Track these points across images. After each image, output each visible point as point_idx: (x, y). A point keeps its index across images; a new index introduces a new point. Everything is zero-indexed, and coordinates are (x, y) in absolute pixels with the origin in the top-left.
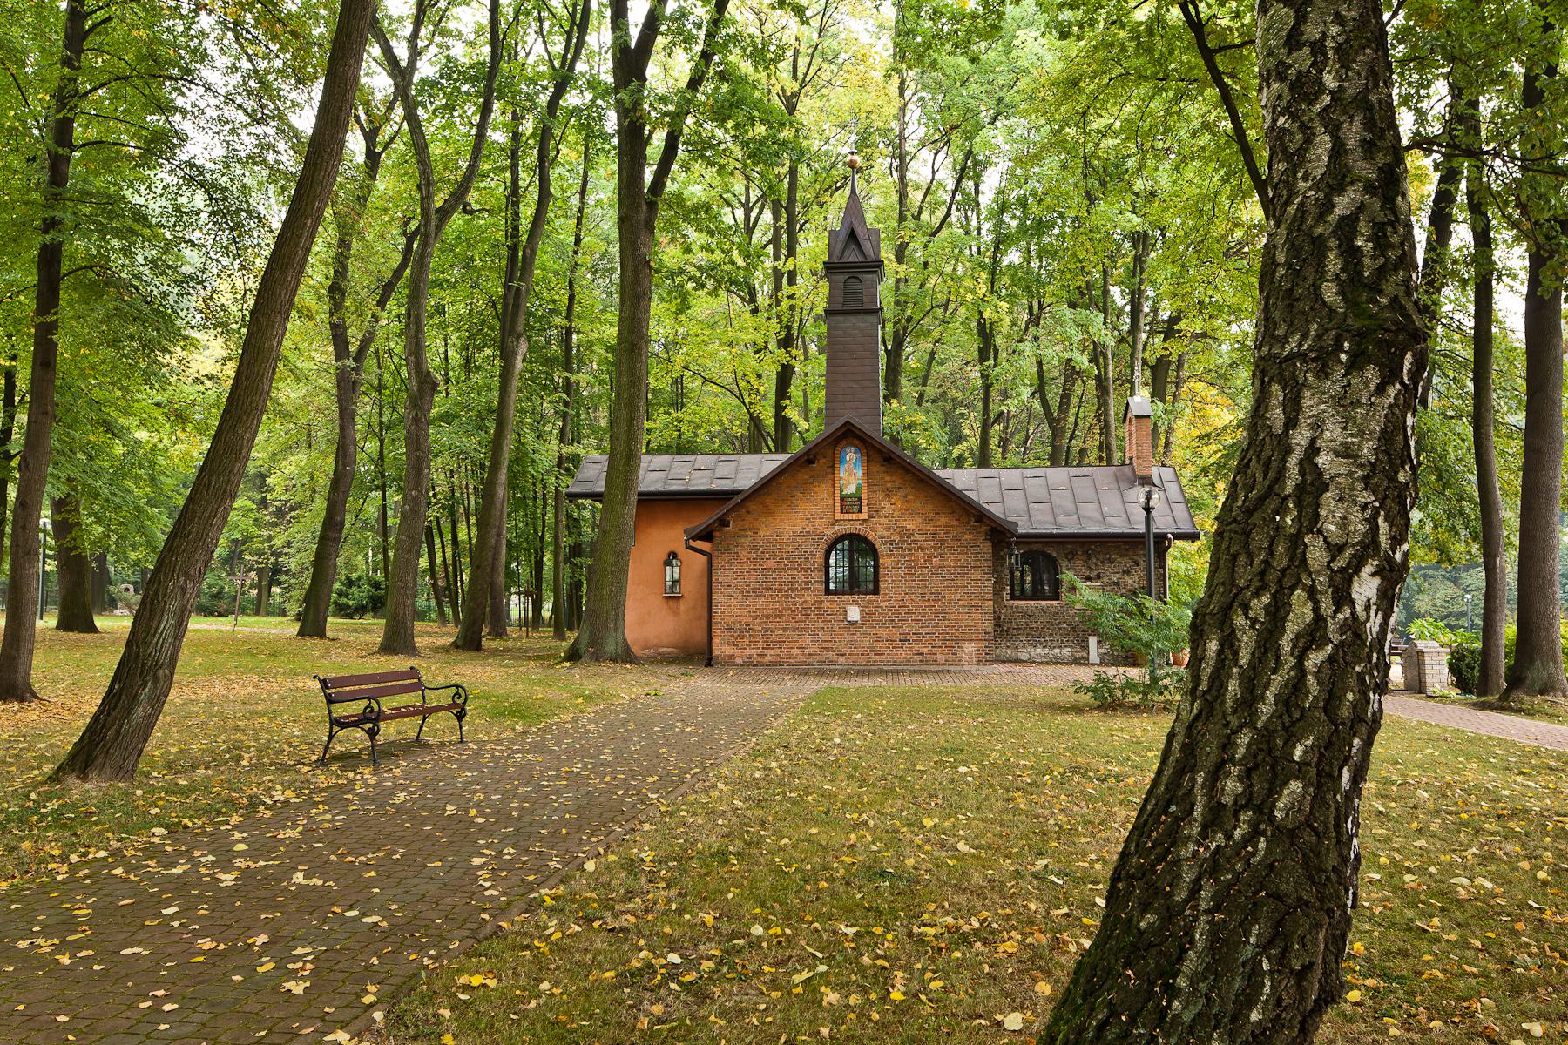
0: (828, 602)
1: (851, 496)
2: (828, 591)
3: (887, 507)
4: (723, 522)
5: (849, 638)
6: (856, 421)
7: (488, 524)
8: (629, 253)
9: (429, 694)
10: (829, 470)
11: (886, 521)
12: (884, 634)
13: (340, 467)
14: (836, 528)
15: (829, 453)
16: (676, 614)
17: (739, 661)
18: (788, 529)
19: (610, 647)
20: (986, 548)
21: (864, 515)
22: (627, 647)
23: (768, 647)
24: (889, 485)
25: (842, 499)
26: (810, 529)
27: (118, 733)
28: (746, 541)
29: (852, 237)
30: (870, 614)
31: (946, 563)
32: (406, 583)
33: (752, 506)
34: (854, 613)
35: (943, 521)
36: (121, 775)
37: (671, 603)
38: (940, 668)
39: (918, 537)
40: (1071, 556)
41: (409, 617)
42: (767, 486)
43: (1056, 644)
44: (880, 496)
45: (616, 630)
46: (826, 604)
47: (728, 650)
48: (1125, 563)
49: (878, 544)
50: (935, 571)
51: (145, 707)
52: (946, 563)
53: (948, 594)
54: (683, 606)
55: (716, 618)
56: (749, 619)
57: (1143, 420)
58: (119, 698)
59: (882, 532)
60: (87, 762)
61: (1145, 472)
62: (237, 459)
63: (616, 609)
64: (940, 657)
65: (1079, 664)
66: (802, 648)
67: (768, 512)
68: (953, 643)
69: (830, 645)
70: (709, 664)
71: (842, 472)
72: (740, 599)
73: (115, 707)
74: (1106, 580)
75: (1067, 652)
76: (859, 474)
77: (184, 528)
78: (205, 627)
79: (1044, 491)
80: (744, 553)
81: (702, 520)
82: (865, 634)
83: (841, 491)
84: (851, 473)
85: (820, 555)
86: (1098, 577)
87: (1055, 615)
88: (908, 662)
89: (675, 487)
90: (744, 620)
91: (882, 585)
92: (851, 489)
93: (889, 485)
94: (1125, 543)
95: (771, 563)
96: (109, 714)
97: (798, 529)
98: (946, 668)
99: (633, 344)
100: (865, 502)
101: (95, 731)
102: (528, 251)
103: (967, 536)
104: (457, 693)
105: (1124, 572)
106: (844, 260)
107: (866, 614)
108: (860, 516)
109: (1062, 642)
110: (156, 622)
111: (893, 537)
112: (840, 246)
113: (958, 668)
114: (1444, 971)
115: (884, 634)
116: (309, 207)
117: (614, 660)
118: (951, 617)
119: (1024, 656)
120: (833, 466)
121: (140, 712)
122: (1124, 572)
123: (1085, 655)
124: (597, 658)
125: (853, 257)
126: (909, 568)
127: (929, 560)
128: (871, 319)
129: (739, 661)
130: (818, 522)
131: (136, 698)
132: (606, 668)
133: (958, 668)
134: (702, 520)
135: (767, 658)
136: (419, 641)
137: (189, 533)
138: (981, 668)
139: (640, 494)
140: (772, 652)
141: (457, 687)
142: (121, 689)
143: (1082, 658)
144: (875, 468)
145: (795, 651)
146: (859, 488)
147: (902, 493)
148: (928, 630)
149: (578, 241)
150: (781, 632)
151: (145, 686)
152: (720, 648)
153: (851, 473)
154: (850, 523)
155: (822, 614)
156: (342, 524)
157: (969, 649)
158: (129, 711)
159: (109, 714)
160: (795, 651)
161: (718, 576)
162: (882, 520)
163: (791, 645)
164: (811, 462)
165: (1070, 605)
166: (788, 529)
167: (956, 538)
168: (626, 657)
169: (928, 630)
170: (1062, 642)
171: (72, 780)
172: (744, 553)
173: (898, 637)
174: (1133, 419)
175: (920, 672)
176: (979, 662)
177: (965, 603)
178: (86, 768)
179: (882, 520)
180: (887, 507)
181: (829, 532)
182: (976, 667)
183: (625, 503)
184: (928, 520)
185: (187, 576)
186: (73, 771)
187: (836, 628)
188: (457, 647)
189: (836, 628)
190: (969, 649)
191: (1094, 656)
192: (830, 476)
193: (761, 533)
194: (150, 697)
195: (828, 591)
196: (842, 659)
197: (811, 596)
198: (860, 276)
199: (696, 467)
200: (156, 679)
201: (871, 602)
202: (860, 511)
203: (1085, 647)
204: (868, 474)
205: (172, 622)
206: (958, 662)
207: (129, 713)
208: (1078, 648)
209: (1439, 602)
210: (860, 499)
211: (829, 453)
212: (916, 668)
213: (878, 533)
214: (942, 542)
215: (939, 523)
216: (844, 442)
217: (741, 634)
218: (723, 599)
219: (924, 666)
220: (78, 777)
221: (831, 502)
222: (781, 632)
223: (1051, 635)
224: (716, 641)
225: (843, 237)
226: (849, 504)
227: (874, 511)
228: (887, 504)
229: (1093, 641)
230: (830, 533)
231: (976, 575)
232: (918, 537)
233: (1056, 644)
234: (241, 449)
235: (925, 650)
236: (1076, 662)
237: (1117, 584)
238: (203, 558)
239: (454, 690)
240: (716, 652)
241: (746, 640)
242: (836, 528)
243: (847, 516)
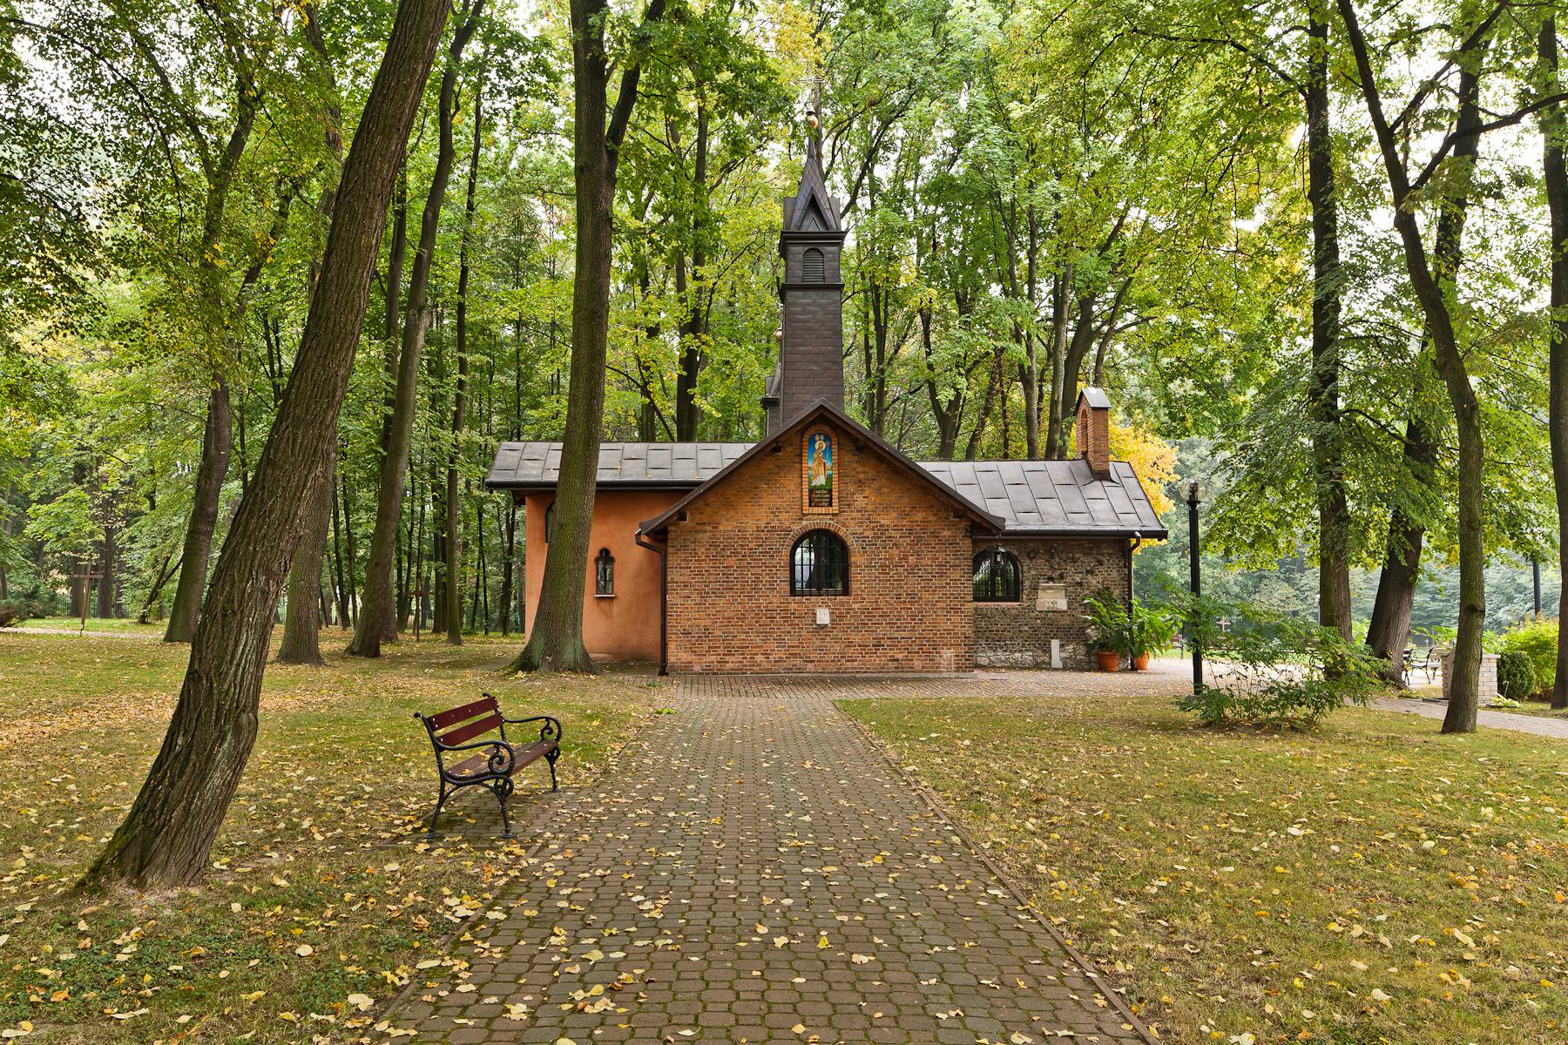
0: (794, 604)
1: (820, 488)
2: (793, 592)
3: (860, 500)
4: (681, 516)
5: (818, 643)
6: (829, 405)
7: (387, 517)
8: (588, 207)
9: (510, 729)
10: (797, 459)
11: (859, 515)
12: (856, 638)
13: (213, 452)
14: (804, 523)
15: (796, 441)
16: (609, 616)
17: (697, 668)
18: (751, 525)
19: (569, 655)
20: (966, 545)
21: (835, 509)
22: (585, 654)
23: (730, 654)
24: (861, 476)
25: (811, 491)
26: (776, 523)
27: (187, 811)
28: (705, 537)
29: (814, 205)
30: (841, 616)
31: (923, 562)
32: (310, 582)
33: (711, 499)
34: (823, 616)
35: (919, 516)
36: (189, 877)
37: (603, 604)
38: (917, 675)
39: (893, 533)
40: (1032, 555)
41: (313, 621)
42: (730, 477)
43: (1017, 648)
44: (852, 488)
45: (574, 635)
46: (793, 606)
47: (685, 657)
48: (1089, 562)
49: (851, 542)
50: (912, 571)
51: (223, 771)
52: (923, 562)
53: (926, 595)
54: (616, 608)
55: (671, 622)
56: (708, 623)
57: (1101, 413)
58: (187, 759)
59: (853, 528)
60: (142, 857)
61: (1102, 468)
62: (330, 405)
63: (575, 612)
64: (917, 664)
65: (1041, 669)
66: (766, 655)
67: (729, 505)
68: (930, 649)
69: (797, 651)
70: (663, 673)
71: (810, 463)
72: (698, 600)
73: (181, 773)
74: (1069, 580)
75: (1028, 656)
76: (829, 465)
77: (263, 503)
78: (41, 631)
79: (999, 485)
80: (703, 550)
81: (658, 514)
82: (836, 640)
83: (810, 482)
84: (819, 467)
85: (786, 552)
86: (1061, 577)
87: (1016, 617)
88: (882, 669)
89: (654, 476)
90: (702, 623)
91: (854, 586)
92: (820, 480)
93: (861, 476)
94: (1089, 541)
95: (732, 561)
96: (172, 784)
97: (762, 524)
98: (923, 675)
99: (593, 312)
100: (835, 495)
101: (153, 811)
102: (430, 214)
103: (946, 533)
104: (547, 727)
105: (1088, 572)
106: (803, 230)
107: (837, 617)
108: (830, 510)
109: (1023, 646)
110: (232, 643)
111: (867, 533)
112: (798, 214)
113: (937, 675)
114: (1352, 969)
115: (856, 638)
116: (420, 46)
117: (573, 669)
118: (928, 621)
119: (983, 661)
120: (800, 455)
121: (216, 779)
122: (1088, 572)
123: (1047, 660)
124: (556, 667)
125: (811, 226)
126: (883, 567)
127: (905, 558)
128: (835, 295)
129: (697, 668)
130: (783, 516)
131: (210, 757)
132: (567, 678)
133: (937, 675)
134: (658, 514)
135: (730, 666)
136: (324, 647)
137: (271, 512)
138: (961, 675)
139: (600, 484)
140: (733, 659)
141: (548, 719)
142: (189, 747)
143: (1044, 662)
144: (846, 459)
145: (759, 658)
146: (829, 479)
147: (875, 485)
148: (904, 634)
149: (470, 207)
150: (743, 636)
151: (223, 740)
152: (676, 655)
153: (819, 467)
154: (819, 518)
155: (788, 616)
156: (215, 515)
157: (948, 654)
158: (202, 777)
159: (172, 784)
160: (759, 658)
161: (673, 575)
162: (854, 514)
163: (755, 651)
164: (777, 449)
165: (1032, 608)
166: (751, 525)
167: (935, 535)
168: (586, 666)
169: (904, 634)
170: (1023, 646)
171: (121, 889)
172: (703, 550)
173: (871, 642)
174: (1090, 414)
175: (894, 681)
176: (958, 669)
177: (943, 605)
178: (142, 868)
179: (854, 514)
180: (860, 500)
181: (796, 527)
182: (954, 675)
183: (584, 492)
184: (903, 515)
185: (269, 574)
186: (122, 875)
187: (804, 633)
188: (354, 653)
189: (804, 633)
190: (948, 654)
191: (1056, 661)
192: (797, 466)
193: (721, 528)
194: (230, 757)
195: (793, 592)
196: (810, 666)
197: (776, 596)
198: (821, 248)
199: (626, 456)
200: (238, 729)
201: (842, 604)
202: (830, 504)
203: (1048, 651)
204: (840, 465)
205: (253, 642)
206: (937, 669)
207: (203, 779)
208: (1040, 653)
209: (1275, 601)
210: (830, 491)
211: (796, 441)
212: (892, 675)
213: (850, 530)
214: (919, 539)
215: (915, 519)
216: (812, 430)
217: (699, 639)
218: (679, 601)
219: (900, 674)
220: (130, 883)
221: (798, 495)
222: (743, 636)
223: (1011, 639)
224: (672, 647)
225: (802, 203)
226: (818, 497)
227: (846, 504)
228: (859, 497)
229: (1055, 644)
230: (797, 528)
231: (956, 575)
232: (893, 533)
233: (1017, 648)
234: (335, 390)
235: (900, 656)
236: (1037, 667)
237: (1080, 584)
238: (290, 547)
239: (541, 724)
240: (672, 659)
241: (705, 647)
242: (804, 523)
243: (816, 510)
